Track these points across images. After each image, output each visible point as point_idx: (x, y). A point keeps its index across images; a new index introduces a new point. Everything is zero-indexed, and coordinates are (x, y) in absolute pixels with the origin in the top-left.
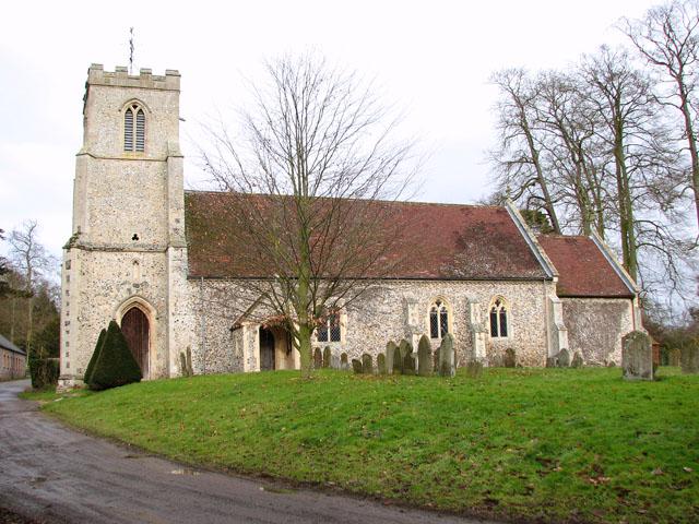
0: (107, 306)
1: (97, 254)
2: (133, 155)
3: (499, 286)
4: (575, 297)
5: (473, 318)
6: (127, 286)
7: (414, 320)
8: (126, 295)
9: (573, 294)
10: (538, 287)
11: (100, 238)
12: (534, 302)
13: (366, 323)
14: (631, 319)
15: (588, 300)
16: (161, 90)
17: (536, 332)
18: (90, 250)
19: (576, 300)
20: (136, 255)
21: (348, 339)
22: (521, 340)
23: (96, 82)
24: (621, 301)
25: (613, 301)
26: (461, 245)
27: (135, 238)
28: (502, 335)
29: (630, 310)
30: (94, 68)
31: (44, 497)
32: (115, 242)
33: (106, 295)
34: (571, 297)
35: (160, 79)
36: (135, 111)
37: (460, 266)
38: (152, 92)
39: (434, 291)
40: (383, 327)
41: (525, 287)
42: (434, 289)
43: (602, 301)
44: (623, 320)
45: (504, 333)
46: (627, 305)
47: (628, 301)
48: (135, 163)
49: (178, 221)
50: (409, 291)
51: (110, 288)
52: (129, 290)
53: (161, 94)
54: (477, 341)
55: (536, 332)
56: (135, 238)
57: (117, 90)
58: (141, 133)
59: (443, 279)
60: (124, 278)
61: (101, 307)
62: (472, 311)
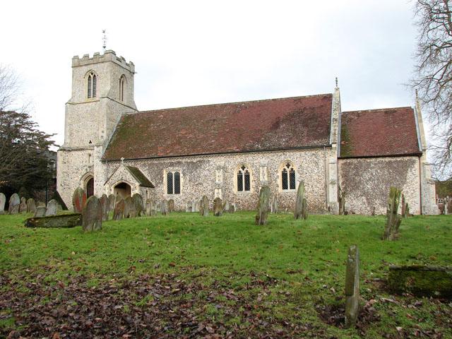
0: (77, 178)
1: (73, 153)
2: (90, 100)
3: (288, 154)
4: (361, 157)
5: (261, 177)
6: (85, 168)
9: (358, 155)
10: (320, 153)
12: (317, 163)
14: (417, 173)
15: (373, 160)
16: (103, 62)
17: (318, 185)
19: (362, 160)
20: (90, 152)
23: (77, 63)
24: (406, 158)
25: (399, 159)
26: (276, 126)
27: (90, 142)
31: (60, 272)
32: (81, 146)
34: (357, 158)
35: (102, 57)
36: (92, 76)
37: (258, 141)
38: (98, 65)
40: (205, 185)
41: (309, 153)
42: (239, 159)
43: (387, 159)
44: (409, 174)
46: (414, 162)
48: (90, 104)
49: (103, 132)
55: (318, 185)
56: (90, 142)
57: (84, 67)
58: (94, 88)
59: (244, 151)
60: (84, 163)
62: (261, 172)
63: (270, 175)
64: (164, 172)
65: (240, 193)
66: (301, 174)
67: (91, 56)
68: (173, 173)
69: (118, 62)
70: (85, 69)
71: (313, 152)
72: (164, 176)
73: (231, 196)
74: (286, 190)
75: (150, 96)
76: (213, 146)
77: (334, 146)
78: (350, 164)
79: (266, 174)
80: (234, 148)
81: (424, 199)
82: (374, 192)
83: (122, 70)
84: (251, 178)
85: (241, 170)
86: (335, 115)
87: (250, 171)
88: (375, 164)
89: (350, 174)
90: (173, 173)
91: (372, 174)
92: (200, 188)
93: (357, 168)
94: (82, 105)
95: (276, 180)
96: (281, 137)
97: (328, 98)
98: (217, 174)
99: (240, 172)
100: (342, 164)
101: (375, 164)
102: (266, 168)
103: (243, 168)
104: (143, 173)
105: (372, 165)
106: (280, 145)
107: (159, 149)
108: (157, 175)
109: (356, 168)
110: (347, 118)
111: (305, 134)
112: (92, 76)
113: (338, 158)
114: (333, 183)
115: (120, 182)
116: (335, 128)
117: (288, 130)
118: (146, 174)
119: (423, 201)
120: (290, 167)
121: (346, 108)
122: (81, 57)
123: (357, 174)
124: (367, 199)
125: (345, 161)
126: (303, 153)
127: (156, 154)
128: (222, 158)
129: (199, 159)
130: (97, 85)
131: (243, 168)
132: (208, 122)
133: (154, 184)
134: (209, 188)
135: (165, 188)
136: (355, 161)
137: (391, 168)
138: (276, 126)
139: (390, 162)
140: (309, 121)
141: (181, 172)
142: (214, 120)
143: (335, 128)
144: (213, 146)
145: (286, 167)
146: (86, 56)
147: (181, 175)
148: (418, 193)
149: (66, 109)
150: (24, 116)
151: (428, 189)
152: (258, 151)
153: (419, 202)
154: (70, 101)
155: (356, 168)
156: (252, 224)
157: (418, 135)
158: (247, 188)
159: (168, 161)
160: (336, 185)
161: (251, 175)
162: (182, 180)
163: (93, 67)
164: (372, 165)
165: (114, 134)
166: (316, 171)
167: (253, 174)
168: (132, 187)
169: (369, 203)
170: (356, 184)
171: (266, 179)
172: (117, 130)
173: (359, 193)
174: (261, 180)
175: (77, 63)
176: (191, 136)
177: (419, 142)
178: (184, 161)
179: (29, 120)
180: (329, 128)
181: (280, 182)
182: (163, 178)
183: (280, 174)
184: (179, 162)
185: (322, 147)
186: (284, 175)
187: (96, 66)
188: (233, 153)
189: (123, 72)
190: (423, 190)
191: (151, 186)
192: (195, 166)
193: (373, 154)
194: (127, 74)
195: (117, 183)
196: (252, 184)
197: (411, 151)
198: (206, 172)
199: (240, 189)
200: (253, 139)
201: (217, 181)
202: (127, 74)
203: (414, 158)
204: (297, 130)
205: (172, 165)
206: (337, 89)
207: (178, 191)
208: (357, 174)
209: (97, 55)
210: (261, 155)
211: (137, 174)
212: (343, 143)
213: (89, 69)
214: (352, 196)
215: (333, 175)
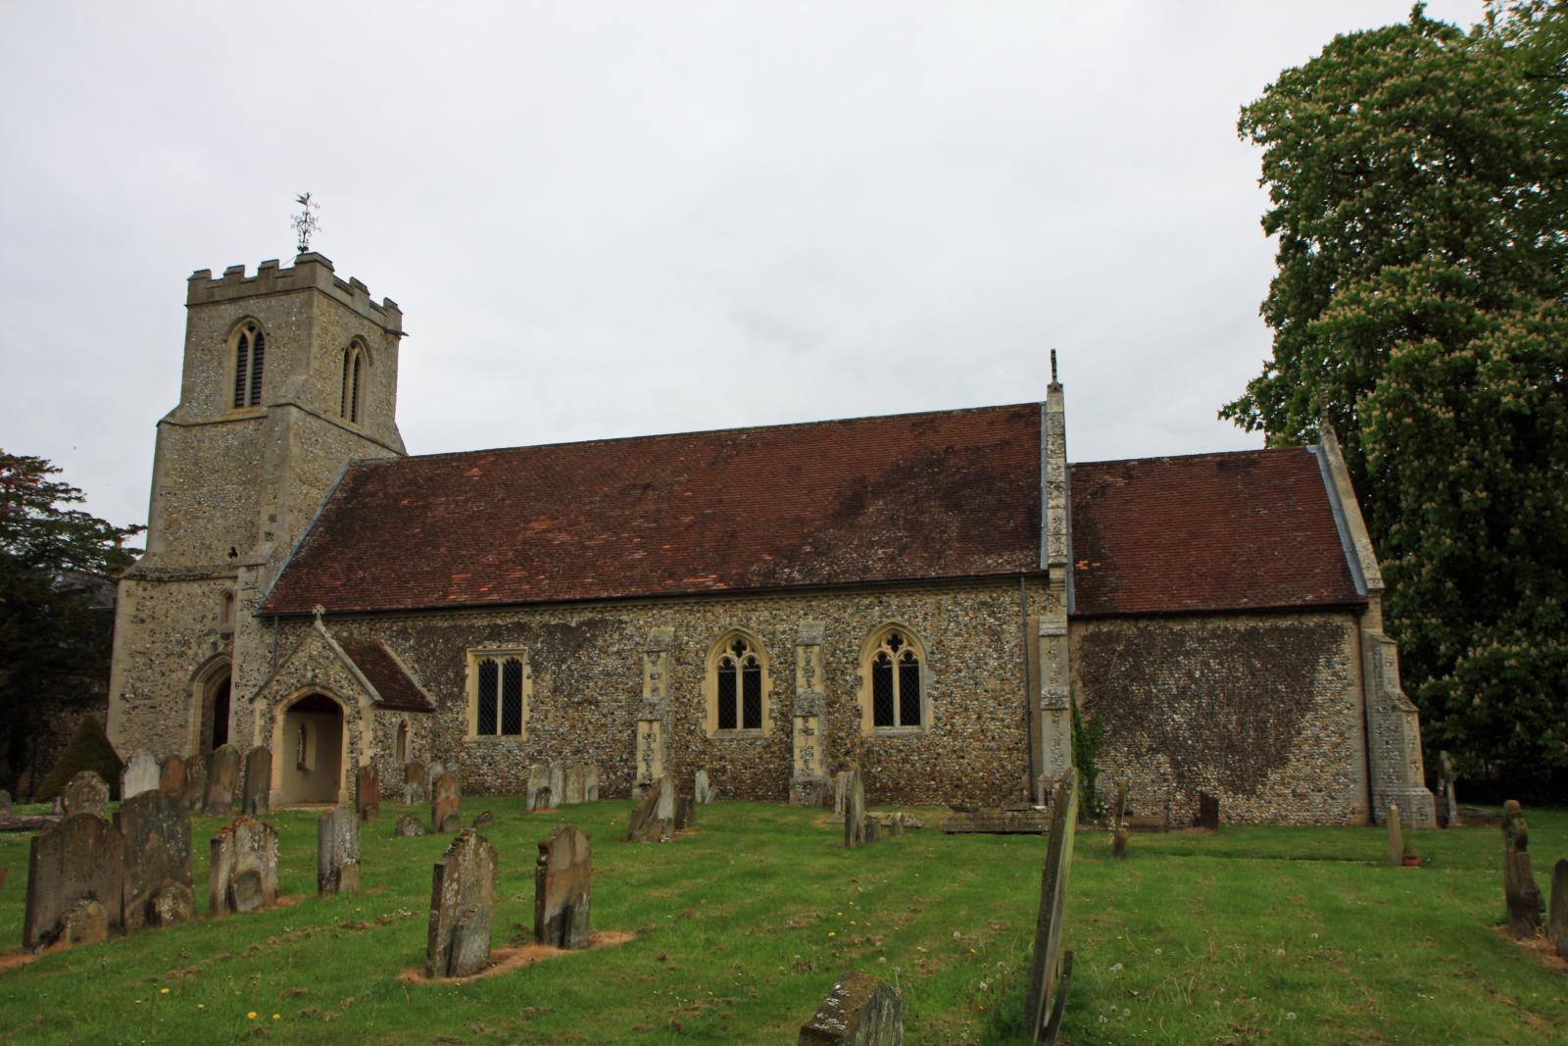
2: (240, 413)
3: (894, 602)
4: (1152, 616)
5: (801, 680)
7: (655, 690)
8: (209, 654)
9: (1141, 607)
11: (182, 559)
12: (996, 636)
13: (569, 696)
14: (1351, 671)
16: (287, 292)
18: (160, 580)
19: (1153, 626)
20: (228, 584)
21: (532, 731)
22: (952, 733)
23: (204, 293)
24: (1311, 621)
26: (851, 506)
27: (233, 554)
28: (505, 732)
29: (1349, 647)
30: (200, 279)
33: (182, 655)
36: (250, 337)
38: (273, 301)
39: (725, 621)
41: (968, 600)
42: (725, 618)
43: (1242, 625)
44: (1324, 675)
45: (911, 716)
46: (1336, 635)
47: (1348, 623)
48: (239, 427)
50: (662, 626)
51: (187, 643)
52: (214, 644)
53: (285, 300)
54: (799, 741)
56: (233, 554)
59: (742, 593)
60: (209, 624)
61: (174, 676)
62: (801, 663)
63: (832, 675)
64: (470, 658)
65: (727, 734)
66: (940, 672)
67: (251, 272)
68: (500, 662)
69: (340, 294)
70: (230, 312)
71: (984, 597)
72: (468, 671)
73: (696, 746)
74: (886, 730)
75: (443, 406)
76: (637, 573)
77: (1055, 574)
78: (1111, 638)
79: (818, 672)
80: (710, 581)
81: (1382, 768)
82: (1198, 738)
83: (354, 321)
84: (767, 684)
85: (730, 654)
86: (1052, 471)
87: (920, 656)
88: (1201, 641)
89: (1113, 673)
90: (500, 662)
91: (1190, 675)
92: (591, 715)
93: (1136, 654)
94: (212, 431)
95: (851, 694)
96: (872, 544)
97: (1026, 417)
98: (648, 668)
99: (727, 661)
100: (1085, 639)
101: (1201, 641)
102: (816, 649)
103: (895, 643)
104: (398, 660)
105: (1190, 645)
106: (866, 569)
107: (456, 577)
108: (447, 667)
109: (1132, 651)
110: (1083, 475)
111: (954, 532)
112: (250, 337)
113: (1072, 619)
114: (1055, 708)
115: (306, 691)
116: (1055, 510)
117: (892, 521)
118: (406, 665)
119: (1378, 774)
120: (747, 653)
121: (1080, 450)
122: (217, 274)
123: (1136, 675)
124: (1175, 764)
125: (1092, 628)
126: (947, 600)
127: (446, 595)
128: (668, 613)
129: (587, 615)
130: (266, 367)
131: (739, 648)
132: (624, 492)
133: (431, 698)
134: (622, 715)
135: (471, 713)
136: (1129, 629)
137: (1257, 655)
138: (851, 506)
139: (1253, 632)
140: (967, 492)
141: (524, 660)
142: (647, 487)
143: (1055, 510)
144: (637, 573)
145: (887, 649)
146: (235, 272)
147: (527, 670)
148: (1355, 742)
149: (159, 433)
150: (35, 466)
151: (1398, 729)
152: (791, 591)
153: (1361, 776)
154: (172, 414)
155: (1132, 651)
156: (839, 847)
157: (1344, 540)
158: (753, 719)
159: (481, 622)
160: (1067, 715)
161: (764, 673)
162: (527, 687)
163: (254, 307)
164: (1190, 645)
165: (316, 527)
166: (993, 663)
167: (771, 672)
168: (347, 710)
169: (1180, 777)
170: (1133, 706)
171: (819, 689)
172: (324, 517)
173: (1147, 742)
174: (800, 691)
175: (204, 293)
176: (564, 537)
177: (1351, 565)
178: (536, 620)
179: (50, 478)
180: (1034, 514)
181: (865, 698)
182: (464, 679)
183: (866, 672)
184: (521, 628)
185: (1012, 580)
186: (881, 673)
187: (263, 304)
188: (705, 597)
189: (356, 327)
190: (1375, 735)
191: (419, 706)
192: (574, 640)
193: (1192, 604)
194: (374, 338)
195: (295, 696)
196: (767, 704)
197: (1326, 595)
198: (612, 663)
199: (726, 720)
200: (775, 551)
201: (647, 694)
202: (374, 338)
203: (1337, 620)
204: (926, 519)
205: (496, 634)
206: (1055, 389)
207: (513, 726)
208: (1136, 675)
209: (268, 268)
210: (800, 606)
211: (373, 663)
212: (1082, 565)
213: (241, 313)
214: (1121, 752)
215: (1056, 682)
